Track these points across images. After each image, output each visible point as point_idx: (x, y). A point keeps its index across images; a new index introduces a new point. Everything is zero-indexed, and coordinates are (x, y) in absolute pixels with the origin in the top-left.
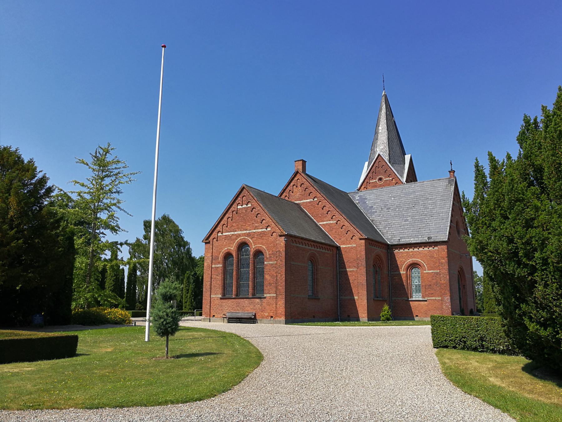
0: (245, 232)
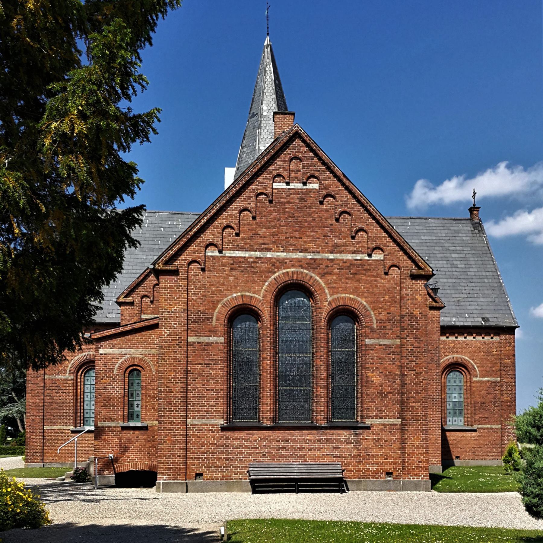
0: (300, 255)
